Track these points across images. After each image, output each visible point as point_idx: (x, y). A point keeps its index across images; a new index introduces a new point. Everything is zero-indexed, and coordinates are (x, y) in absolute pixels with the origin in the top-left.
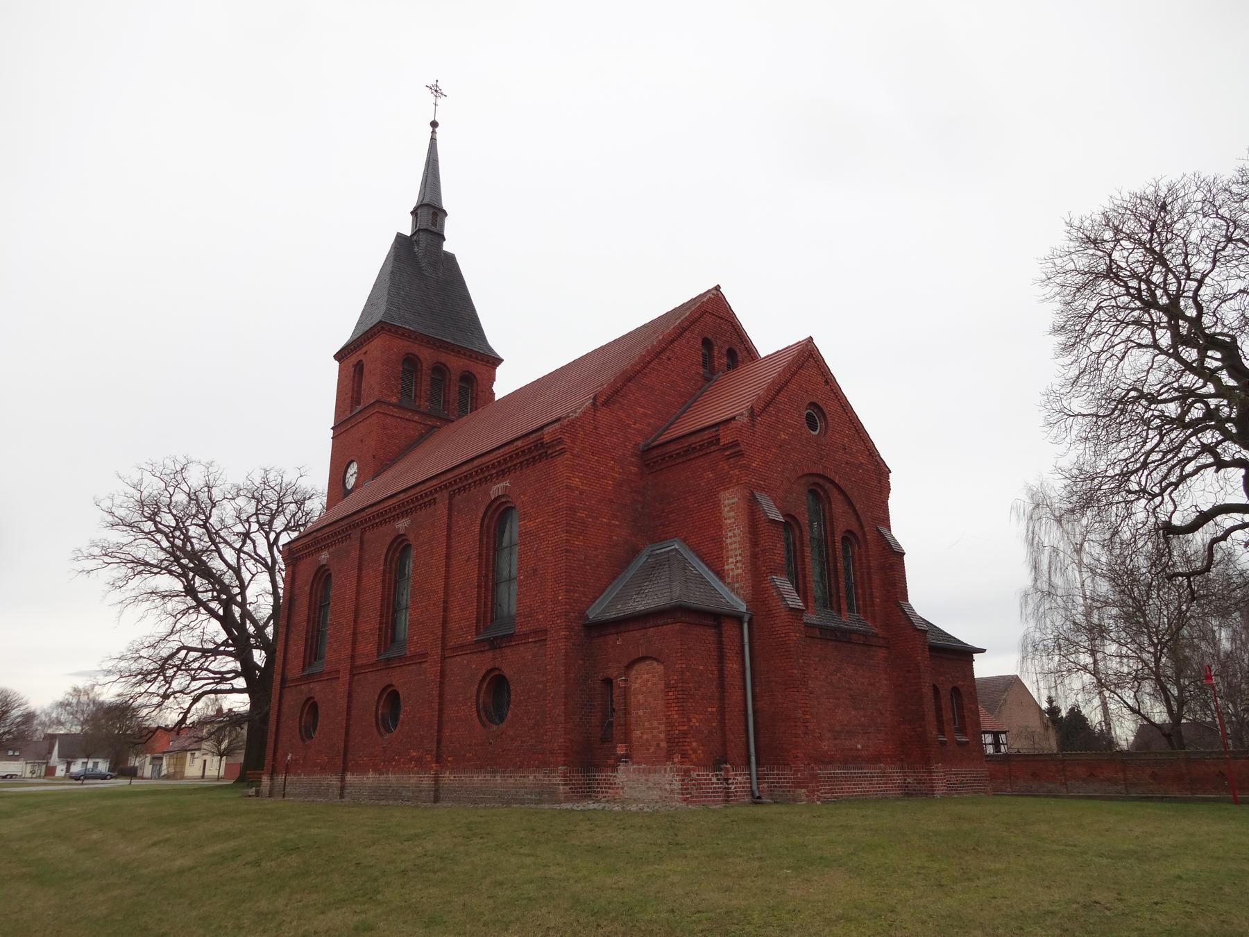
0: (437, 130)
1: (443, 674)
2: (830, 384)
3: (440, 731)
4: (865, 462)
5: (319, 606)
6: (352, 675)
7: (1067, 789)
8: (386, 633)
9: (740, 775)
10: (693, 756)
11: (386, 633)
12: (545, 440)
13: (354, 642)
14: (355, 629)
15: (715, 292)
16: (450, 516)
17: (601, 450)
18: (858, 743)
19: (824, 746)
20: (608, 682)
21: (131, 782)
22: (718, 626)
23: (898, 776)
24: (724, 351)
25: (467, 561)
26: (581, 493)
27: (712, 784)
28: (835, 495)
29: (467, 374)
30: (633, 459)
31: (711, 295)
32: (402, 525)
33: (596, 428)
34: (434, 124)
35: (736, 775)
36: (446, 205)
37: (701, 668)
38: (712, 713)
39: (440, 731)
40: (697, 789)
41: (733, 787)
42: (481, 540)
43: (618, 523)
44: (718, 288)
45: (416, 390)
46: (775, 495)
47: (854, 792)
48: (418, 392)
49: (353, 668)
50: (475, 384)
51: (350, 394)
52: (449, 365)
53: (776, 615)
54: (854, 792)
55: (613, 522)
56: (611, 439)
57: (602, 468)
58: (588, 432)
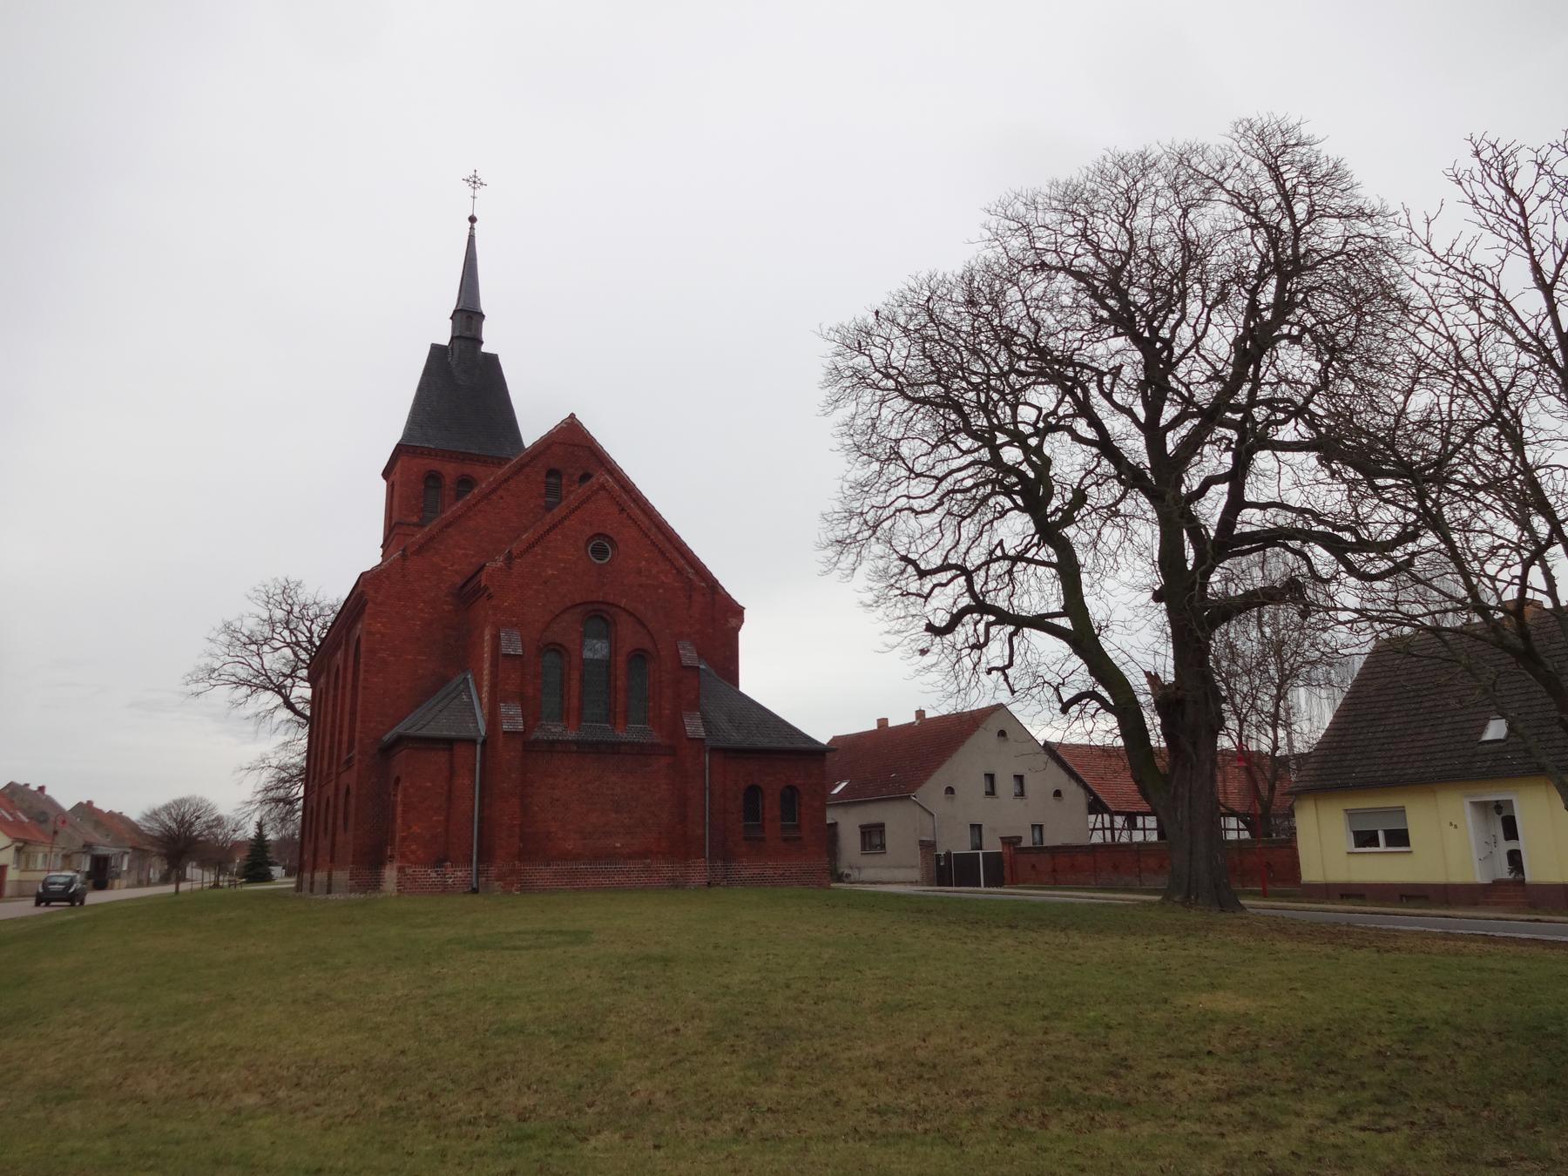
0: (475, 225)
7: (1140, 881)
15: (569, 421)
21: (177, 888)
26: (383, 635)
33: (404, 576)
34: (472, 219)
37: (429, 784)
44: (572, 416)
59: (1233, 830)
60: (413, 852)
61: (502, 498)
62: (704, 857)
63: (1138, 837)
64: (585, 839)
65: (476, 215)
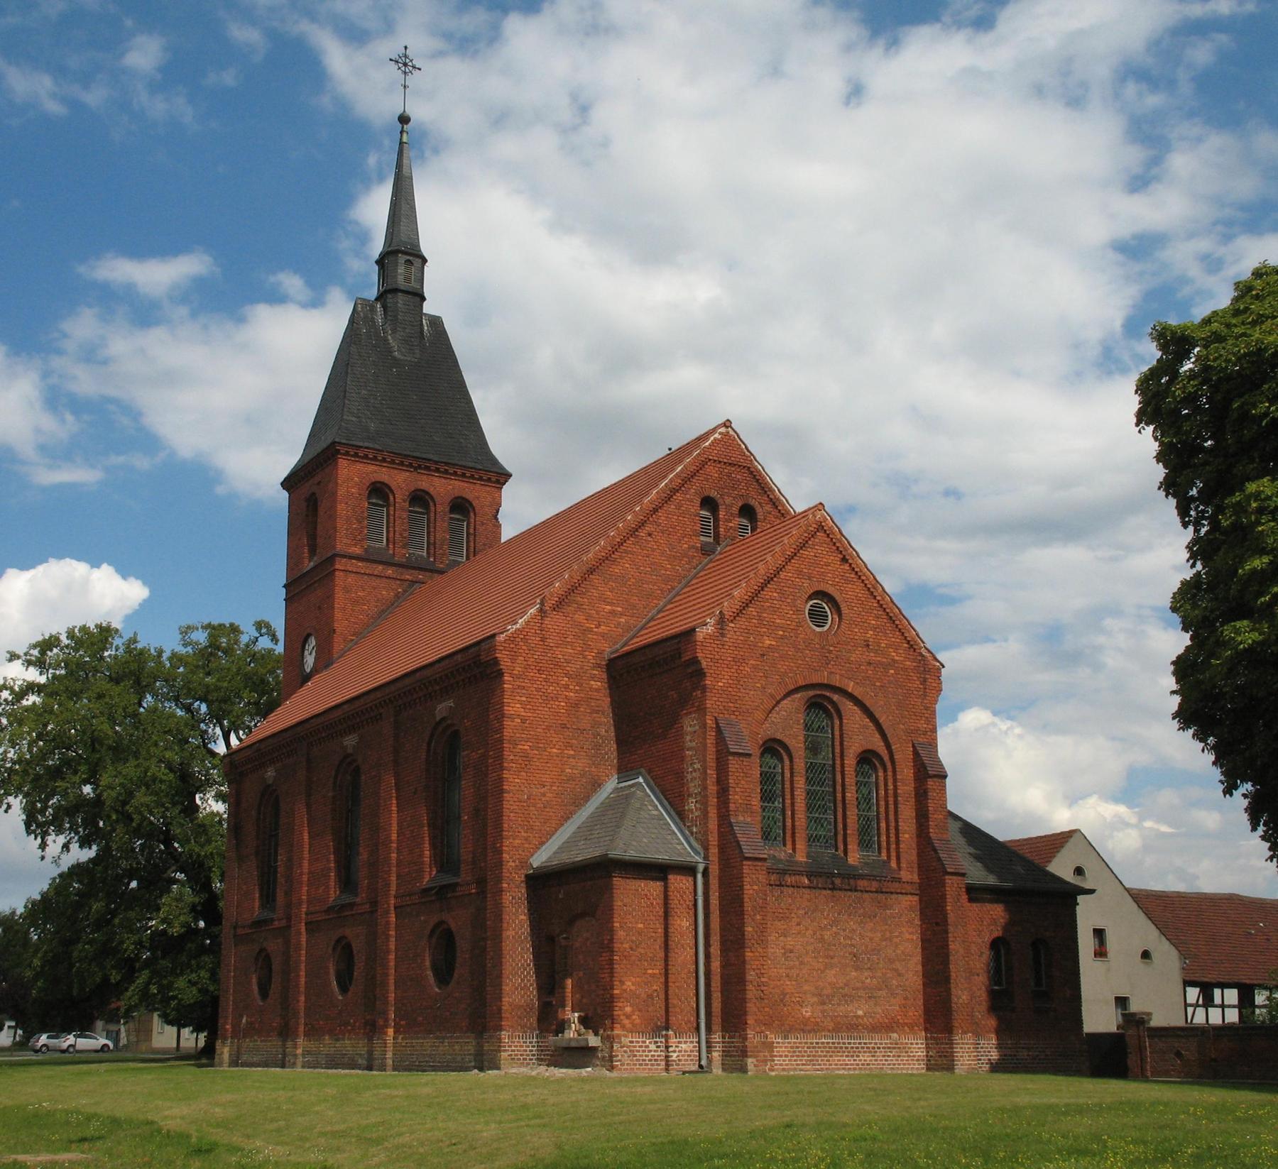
2: (850, 561)
4: (902, 659)
9: (686, 1042)
10: (626, 1022)
12: (481, 657)
15: (723, 430)
18: (859, 1007)
19: (806, 1012)
22: (665, 879)
23: (919, 1048)
24: (735, 510)
25: (415, 793)
27: (650, 1051)
28: (848, 707)
29: (460, 500)
30: (595, 672)
31: (717, 435)
32: (350, 741)
33: (543, 639)
35: (679, 1042)
36: (425, 249)
37: (641, 926)
38: (653, 975)
40: (629, 1057)
41: (675, 1055)
43: (572, 752)
45: (388, 532)
46: (750, 719)
47: (847, 1065)
48: (391, 535)
50: (472, 515)
52: (431, 491)
55: (566, 752)
56: (566, 650)
58: (534, 645)
59: (1229, 1006)
60: (628, 1017)
61: (650, 535)
63: (1215, 1017)
64: (823, 1003)
65: (409, 112)
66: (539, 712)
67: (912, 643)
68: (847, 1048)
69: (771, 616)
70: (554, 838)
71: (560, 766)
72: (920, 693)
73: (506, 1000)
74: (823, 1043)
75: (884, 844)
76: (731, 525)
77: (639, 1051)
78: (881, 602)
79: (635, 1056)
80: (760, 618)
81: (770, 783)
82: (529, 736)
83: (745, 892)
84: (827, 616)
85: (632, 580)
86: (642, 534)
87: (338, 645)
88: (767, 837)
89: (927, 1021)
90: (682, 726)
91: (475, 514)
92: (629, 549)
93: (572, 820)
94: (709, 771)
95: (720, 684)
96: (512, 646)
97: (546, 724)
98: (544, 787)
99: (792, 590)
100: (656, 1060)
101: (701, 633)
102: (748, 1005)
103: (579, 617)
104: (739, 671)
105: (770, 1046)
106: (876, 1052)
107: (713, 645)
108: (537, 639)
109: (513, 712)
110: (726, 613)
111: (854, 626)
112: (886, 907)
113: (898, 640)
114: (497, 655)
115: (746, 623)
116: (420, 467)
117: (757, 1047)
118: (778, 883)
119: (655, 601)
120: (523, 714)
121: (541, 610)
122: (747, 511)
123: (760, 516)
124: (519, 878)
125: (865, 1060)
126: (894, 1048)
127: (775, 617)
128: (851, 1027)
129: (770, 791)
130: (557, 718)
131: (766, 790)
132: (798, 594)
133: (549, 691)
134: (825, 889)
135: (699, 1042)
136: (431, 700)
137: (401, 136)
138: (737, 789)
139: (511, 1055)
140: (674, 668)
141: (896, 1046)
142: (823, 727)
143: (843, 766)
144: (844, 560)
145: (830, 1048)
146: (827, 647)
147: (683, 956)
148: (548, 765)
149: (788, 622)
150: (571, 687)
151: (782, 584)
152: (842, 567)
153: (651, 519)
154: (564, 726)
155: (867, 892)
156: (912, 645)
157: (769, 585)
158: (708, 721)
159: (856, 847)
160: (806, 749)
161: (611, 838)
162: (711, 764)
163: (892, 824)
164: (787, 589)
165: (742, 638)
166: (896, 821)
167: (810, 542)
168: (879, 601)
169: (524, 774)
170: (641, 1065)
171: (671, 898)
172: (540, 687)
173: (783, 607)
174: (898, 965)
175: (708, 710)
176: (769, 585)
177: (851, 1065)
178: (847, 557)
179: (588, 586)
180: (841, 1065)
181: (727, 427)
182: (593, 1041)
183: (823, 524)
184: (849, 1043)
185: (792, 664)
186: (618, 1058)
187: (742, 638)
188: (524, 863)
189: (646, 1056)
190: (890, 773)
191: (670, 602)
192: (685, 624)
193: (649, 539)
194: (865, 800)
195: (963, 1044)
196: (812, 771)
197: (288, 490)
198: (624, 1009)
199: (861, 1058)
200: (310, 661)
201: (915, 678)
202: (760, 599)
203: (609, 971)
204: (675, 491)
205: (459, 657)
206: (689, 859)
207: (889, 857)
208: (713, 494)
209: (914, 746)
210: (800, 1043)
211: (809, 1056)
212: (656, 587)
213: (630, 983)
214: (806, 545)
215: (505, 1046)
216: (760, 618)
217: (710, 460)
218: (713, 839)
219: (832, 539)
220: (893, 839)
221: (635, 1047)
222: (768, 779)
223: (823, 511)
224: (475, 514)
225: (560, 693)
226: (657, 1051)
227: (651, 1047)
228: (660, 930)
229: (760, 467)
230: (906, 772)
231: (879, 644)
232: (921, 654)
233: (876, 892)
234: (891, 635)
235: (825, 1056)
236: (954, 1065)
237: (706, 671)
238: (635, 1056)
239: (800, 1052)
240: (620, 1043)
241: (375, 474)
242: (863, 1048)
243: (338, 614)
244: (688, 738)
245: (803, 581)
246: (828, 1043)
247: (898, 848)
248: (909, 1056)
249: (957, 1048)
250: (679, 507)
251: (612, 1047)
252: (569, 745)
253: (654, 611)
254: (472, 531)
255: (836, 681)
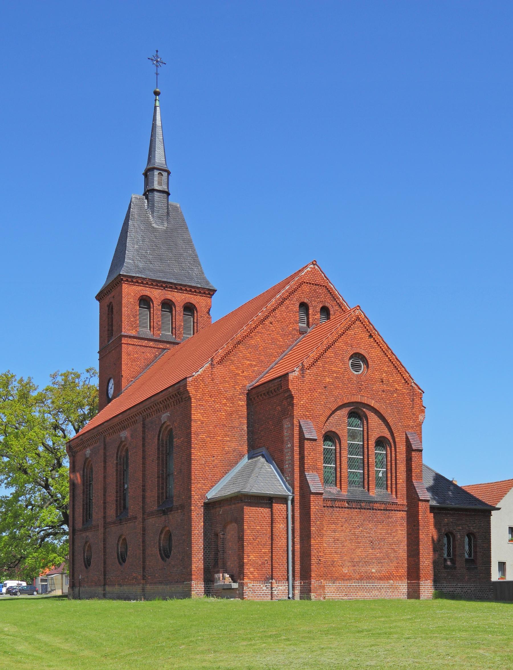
1: (144, 529)
2: (374, 337)
3: (144, 562)
5: (87, 483)
6: (105, 528)
8: (120, 503)
9: (281, 586)
11: (120, 503)
13: (105, 508)
14: (105, 500)
16: (144, 432)
17: (217, 394)
20: (217, 535)
24: (318, 309)
27: (263, 590)
31: (309, 269)
33: (213, 380)
35: (278, 586)
39: (144, 562)
40: (252, 593)
41: (276, 592)
42: (158, 449)
43: (229, 439)
47: (366, 596)
49: (105, 523)
51: (107, 328)
52: (173, 300)
53: (306, 496)
54: (366, 596)
55: (225, 439)
56: (225, 385)
57: (217, 405)
58: (207, 383)
60: (252, 573)
61: (271, 323)
62: (46, 585)
64: (354, 566)
66: (211, 418)
67: (406, 380)
68: (366, 588)
69: (330, 366)
70: (219, 483)
71: (222, 446)
72: (410, 407)
73: (193, 567)
74: (353, 586)
75: (389, 485)
76: (316, 317)
77: (257, 590)
78: (390, 359)
79: (255, 592)
80: (324, 367)
81: (329, 454)
82: (205, 431)
83: (311, 510)
84: (361, 366)
85: (261, 347)
86: (266, 323)
87: (124, 382)
88: (327, 482)
89: (408, 574)
90: (283, 425)
91: (197, 312)
92: (260, 331)
93: (228, 474)
94: (295, 448)
95: (302, 402)
96: (195, 383)
97: (214, 424)
98: (214, 457)
99: (341, 352)
100: (266, 595)
101: (291, 376)
102: (312, 567)
103: (232, 367)
104: (312, 396)
105: (323, 587)
106: (381, 590)
107: (298, 382)
108: (210, 379)
109: (197, 419)
110: (305, 365)
111: (375, 371)
112: (389, 517)
113: (399, 379)
114: (188, 388)
115: (316, 370)
116: (167, 287)
117: (316, 588)
118: (332, 505)
119: (273, 359)
120: (202, 419)
121: (211, 364)
122: (325, 311)
123: (332, 312)
124: (201, 504)
125: (375, 594)
126: (391, 588)
127: (332, 366)
128: (369, 577)
129: (329, 458)
130: (220, 421)
131: (327, 458)
132: (345, 355)
133: (216, 407)
134: (356, 508)
135: (288, 586)
136: (159, 412)
137: (155, 102)
138: (309, 457)
139: (197, 593)
140: (279, 394)
141: (391, 587)
142: (359, 424)
143: (368, 444)
144: (371, 336)
145: (357, 588)
146: (360, 383)
147: (280, 543)
148: (215, 445)
149: (340, 370)
150: (228, 405)
151: (336, 349)
152: (370, 340)
153: (272, 315)
154: (224, 425)
155: (379, 510)
156: (407, 381)
157: (329, 350)
158: (295, 422)
159: (374, 487)
160: (349, 436)
161: (245, 483)
162: (296, 444)
163: (394, 475)
164: (339, 352)
165: (314, 378)
166: (396, 473)
167: (352, 327)
168: (389, 358)
169: (203, 450)
170: (258, 597)
171: (274, 513)
172: (211, 405)
173: (336, 361)
174: (394, 546)
175: (295, 416)
176: (329, 350)
177: (368, 596)
178: (372, 334)
179: (237, 351)
180: (362, 596)
181: (314, 264)
182: (235, 586)
183: (359, 317)
184: (367, 586)
185: (341, 392)
186: (246, 594)
187: (314, 378)
188: (203, 496)
189: (261, 593)
190: (393, 449)
191: (282, 359)
192: (285, 371)
193: (271, 325)
194: (380, 462)
195: (425, 585)
196: (352, 447)
197: (99, 301)
198: (248, 570)
199: (373, 593)
200: (111, 392)
201: (408, 399)
202: (324, 357)
203: (242, 550)
204: (285, 299)
205: (170, 389)
206: (284, 493)
207: (392, 491)
208: (306, 301)
209: (406, 435)
210: (341, 586)
211: (346, 592)
212: (274, 351)
213: (253, 557)
214: (350, 328)
215: (194, 589)
216: (324, 367)
217: (304, 282)
218: (297, 484)
219: (364, 325)
220: (394, 482)
221: (255, 588)
222: (328, 452)
223: (359, 310)
224: (197, 312)
225: (221, 408)
226: (267, 590)
227: (264, 588)
228: (269, 530)
229: (332, 286)
230: (402, 448)
231: (388, 381)
232: (411, 386)
233: (384, 510)
234: (396, 376)
235: (354, 592)
236: (420, 596)
237: (293, 395)
238: (255, 592)
239: (342, 590)
240: (248, 586)
241: (142, 291)
242: (375, 588)
243: (124, 367)
244: (285, 431)
245: (347, 347)
246: (356, 586)
247: (396, 487)
248: (398, 592)
249: (422, 588)
250: (287, 308)
251: (243, 588)
252: (226, 435)
253: (273, 364)
254: (195, 321)
255: (365, 400)
